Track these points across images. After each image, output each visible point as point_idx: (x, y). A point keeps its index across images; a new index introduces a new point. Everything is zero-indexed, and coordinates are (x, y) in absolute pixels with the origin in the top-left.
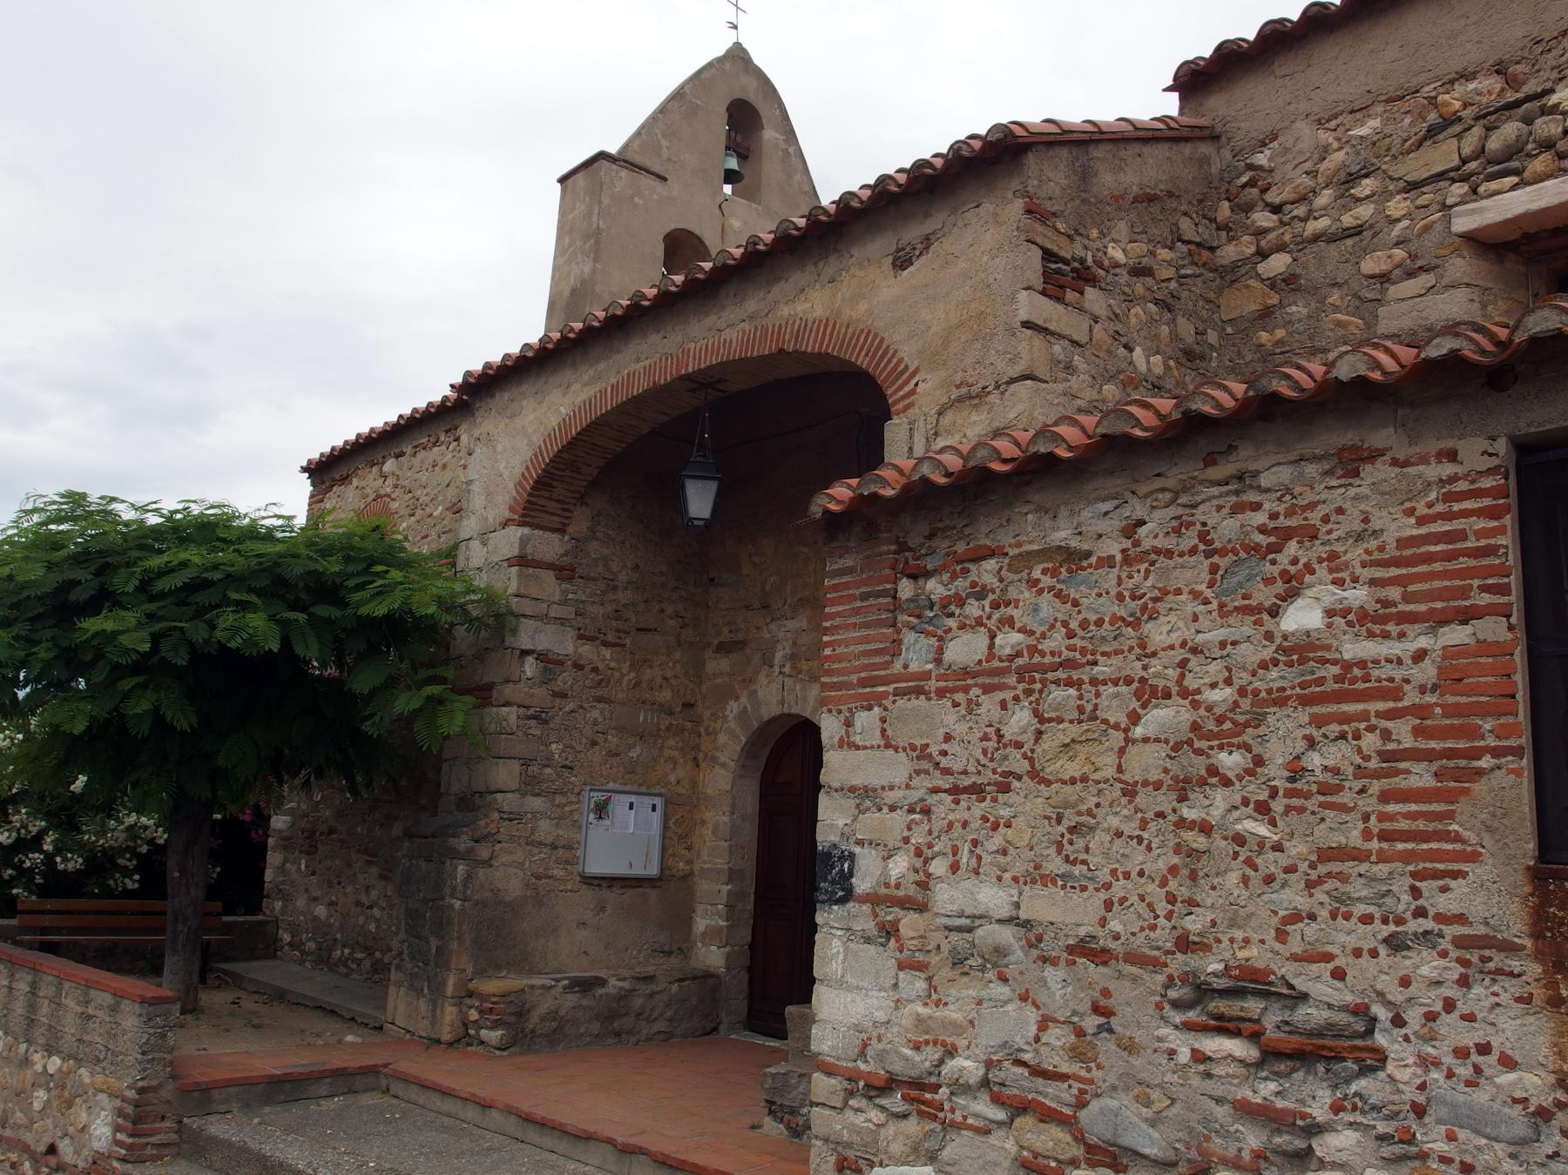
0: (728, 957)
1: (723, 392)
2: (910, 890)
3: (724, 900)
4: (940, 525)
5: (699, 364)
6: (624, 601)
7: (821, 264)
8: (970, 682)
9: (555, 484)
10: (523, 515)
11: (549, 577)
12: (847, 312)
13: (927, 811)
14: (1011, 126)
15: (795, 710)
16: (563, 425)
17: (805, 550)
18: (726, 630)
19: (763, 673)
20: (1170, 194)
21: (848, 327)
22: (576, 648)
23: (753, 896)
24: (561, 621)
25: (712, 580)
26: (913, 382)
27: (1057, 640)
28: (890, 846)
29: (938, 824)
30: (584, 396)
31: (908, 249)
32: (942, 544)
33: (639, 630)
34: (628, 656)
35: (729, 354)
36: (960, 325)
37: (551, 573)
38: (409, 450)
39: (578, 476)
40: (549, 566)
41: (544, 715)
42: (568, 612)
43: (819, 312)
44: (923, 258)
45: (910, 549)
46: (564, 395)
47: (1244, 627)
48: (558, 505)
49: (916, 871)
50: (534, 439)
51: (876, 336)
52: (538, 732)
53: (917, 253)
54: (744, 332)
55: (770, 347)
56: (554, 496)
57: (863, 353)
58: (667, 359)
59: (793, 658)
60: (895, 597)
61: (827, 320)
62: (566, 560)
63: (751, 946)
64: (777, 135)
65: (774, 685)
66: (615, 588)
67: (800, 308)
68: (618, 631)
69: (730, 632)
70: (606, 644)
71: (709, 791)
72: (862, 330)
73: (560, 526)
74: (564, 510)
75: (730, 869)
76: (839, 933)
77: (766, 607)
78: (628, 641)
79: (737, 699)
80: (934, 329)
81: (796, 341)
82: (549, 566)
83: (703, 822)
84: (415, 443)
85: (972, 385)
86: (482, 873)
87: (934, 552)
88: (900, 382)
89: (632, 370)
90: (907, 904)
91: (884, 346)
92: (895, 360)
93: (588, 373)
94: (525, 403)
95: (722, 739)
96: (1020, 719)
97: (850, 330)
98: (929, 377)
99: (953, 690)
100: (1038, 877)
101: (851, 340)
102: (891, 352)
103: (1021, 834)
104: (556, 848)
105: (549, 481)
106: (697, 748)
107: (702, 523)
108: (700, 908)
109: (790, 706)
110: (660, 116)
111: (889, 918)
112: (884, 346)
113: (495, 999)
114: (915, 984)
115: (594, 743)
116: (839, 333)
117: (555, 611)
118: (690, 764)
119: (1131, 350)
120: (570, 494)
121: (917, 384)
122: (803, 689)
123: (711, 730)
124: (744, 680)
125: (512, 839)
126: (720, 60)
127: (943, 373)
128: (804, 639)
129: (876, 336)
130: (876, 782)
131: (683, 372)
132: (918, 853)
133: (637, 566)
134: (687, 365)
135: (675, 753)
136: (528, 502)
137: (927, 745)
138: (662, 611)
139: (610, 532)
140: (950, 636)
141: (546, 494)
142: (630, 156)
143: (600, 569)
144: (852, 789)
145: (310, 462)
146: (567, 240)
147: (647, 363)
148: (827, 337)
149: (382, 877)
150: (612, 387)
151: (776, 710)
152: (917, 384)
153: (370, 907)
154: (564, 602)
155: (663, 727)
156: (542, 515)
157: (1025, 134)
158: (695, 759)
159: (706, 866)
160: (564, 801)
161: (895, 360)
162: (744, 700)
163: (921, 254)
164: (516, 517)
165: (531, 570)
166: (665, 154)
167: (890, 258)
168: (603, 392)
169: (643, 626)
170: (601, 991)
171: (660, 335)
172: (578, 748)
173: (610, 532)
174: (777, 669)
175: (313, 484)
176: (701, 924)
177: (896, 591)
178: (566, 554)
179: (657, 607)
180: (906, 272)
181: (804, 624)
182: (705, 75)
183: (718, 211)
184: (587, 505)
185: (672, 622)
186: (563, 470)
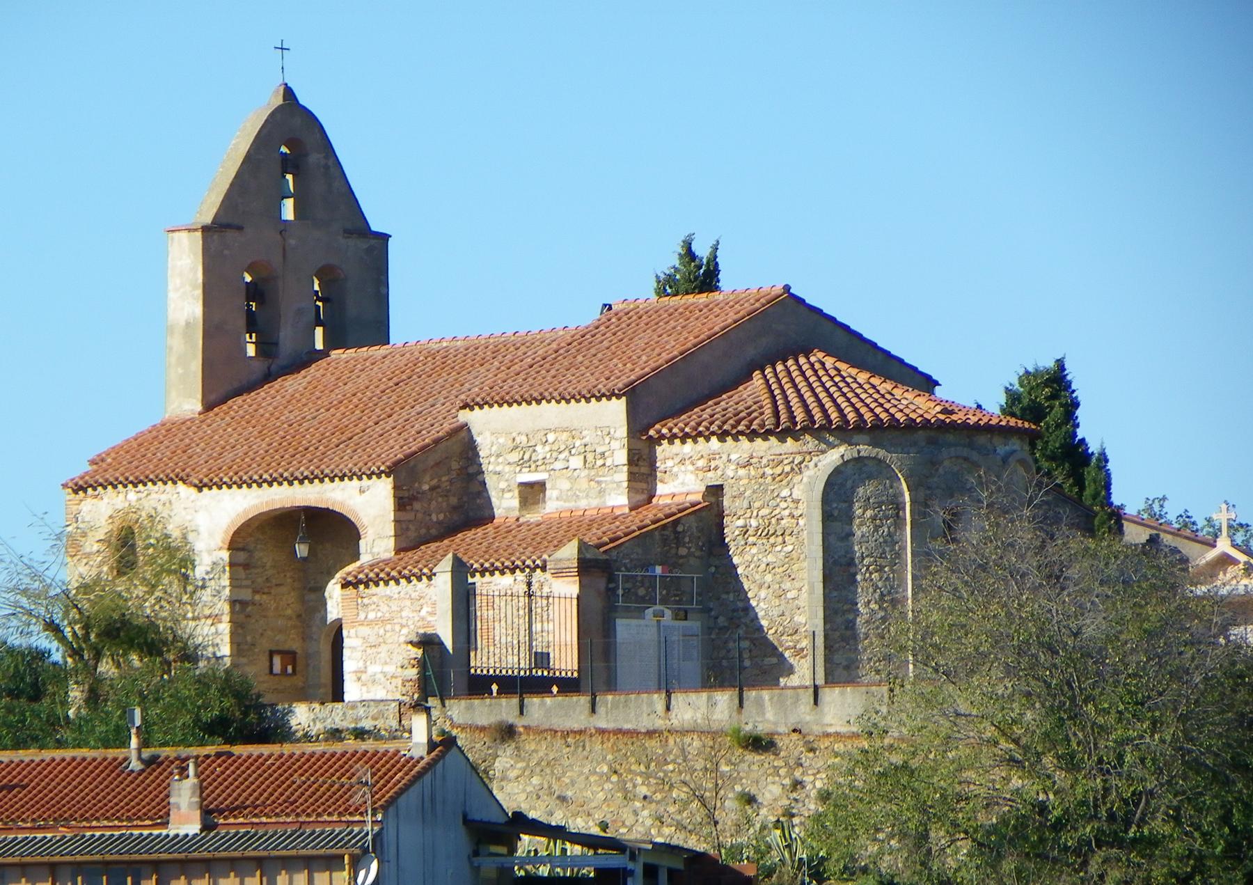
2: (363, 669)
11: (240, 569)
14: (836, 442)
20: (447, 458)
27: (387, 615)
47: (415, 614)
96: (382, 632)
100: (386, 663)
103: (383, 655)
114: (364, 689)
119: (430, 515)
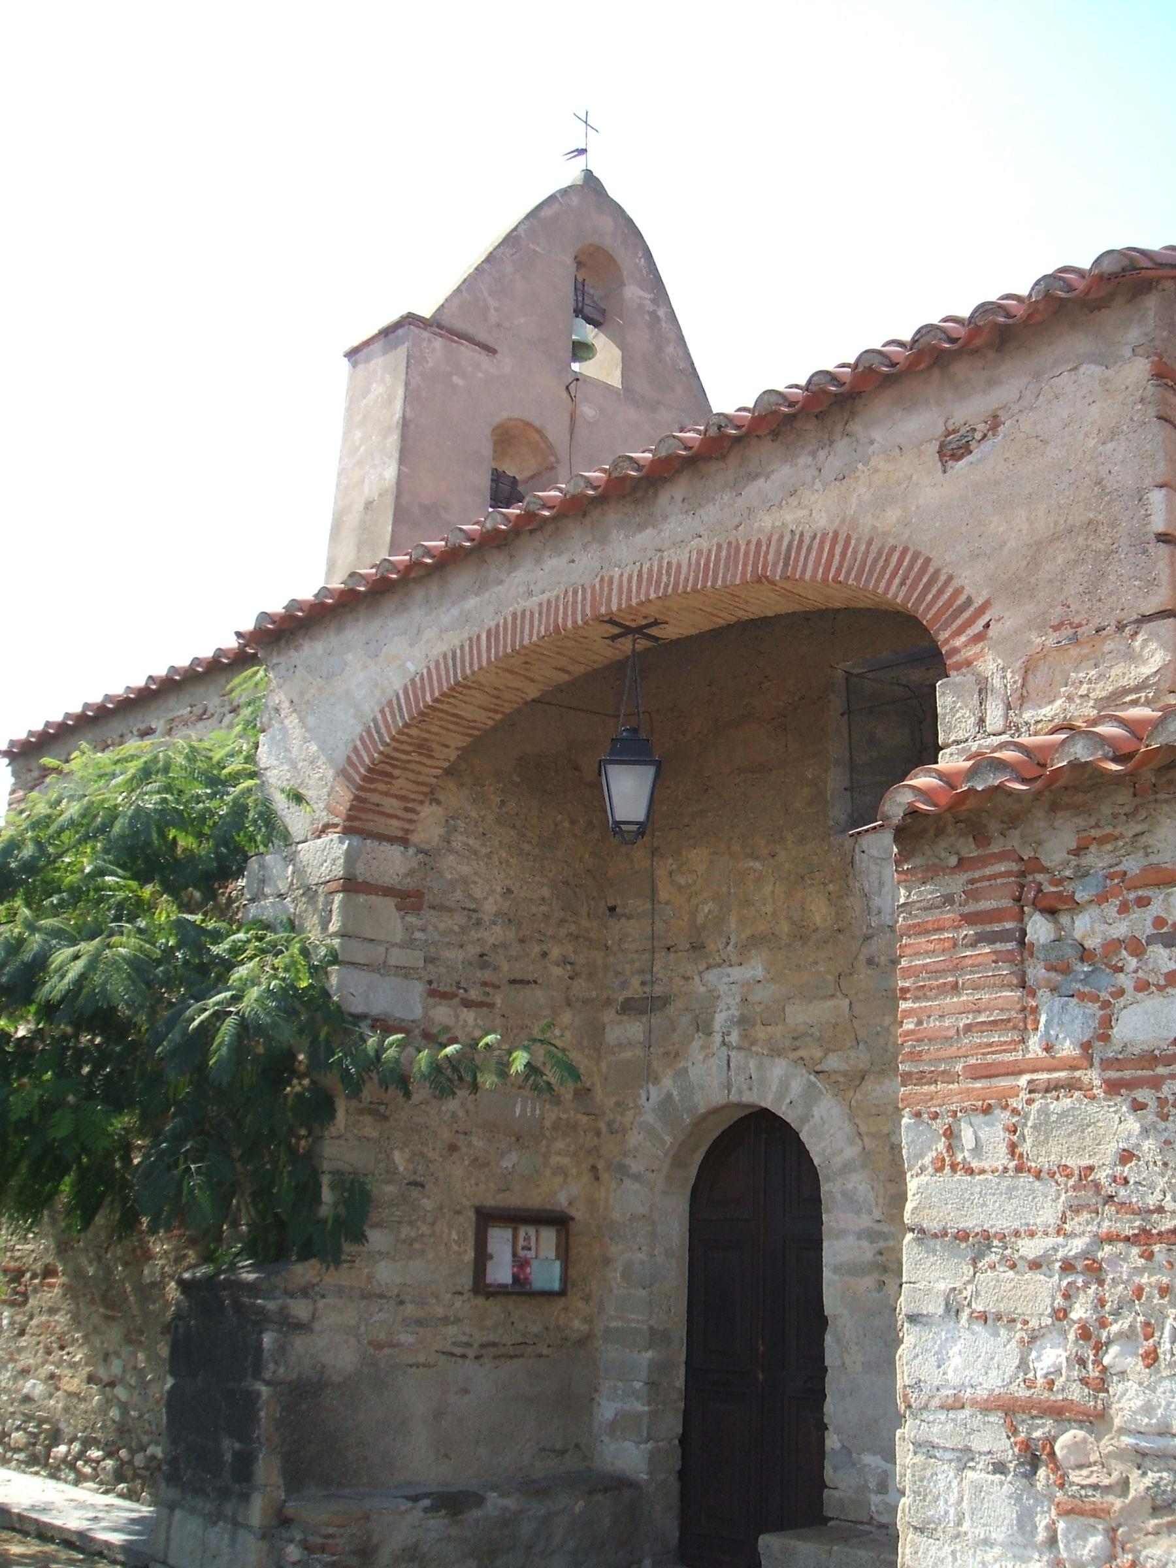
0: (652, 1457)
1: (656, 639)
3: (644, 1375)
4: (1094, 833)
5: (629, 598)
6: (492, 941)
7: (822, 454)
8: (1161, 1070)
9: (396, 772)
10: (350, 818)
11: (387, 905)
12: (867, 522)
13: (1095, 1271)
15: (750, 1097)
16: (414, 686)
17: (758, 865)
18: (635, 981)
19: (696, 1044)
21: (869, 544)
22: (426, 1009)
23: (682, 1370)
24: (405, 972)
25: (612, 909)
26: (982, 622)
28: (1033, 1323)
29: (1113, 1294)
30: (441, 648)
31: (963, 431)
32: (1097, 860)
33: (513, 982)
34: (498, 1021)
35: (676, 584)
36: (1054, 538)
37: (390, 902)
38: (159, 724)
39: (428, 762)
40: (388, 891)
41: (382, 1108)
42: (415, 958)
43: (822, 521)
44: (986, 446)
45: (1045, 870)
46: (412, 645)
48: (401, 804)
49: (1082, 1362)
50: (366, 708)
51: (916, 556)
52: (375, 1134)
53: (978, 436)
54: (700, 552)
55: (744, 574)
56: (394, 790)
57: (897, 581)
58: (575, 593)
59: (744, 1022)
60: (1022, 943)
61: (836, 534)
62: (410, 884)
63: (684, 1440)
64: (641, 293)
65: (713, 1061)
66: (479, 923)
67: (790, 517)
68: (484, 984)
69: (643, 983)
70: (467, 1004)
71: (616, 1215)
72: (894, 548)
73: (400, 834)
74: (406, 809)
75: (651, 1328)
76: (949, 1455)
77: (697, 947)
78: (498, 1000)
79: (656, 1080)
80: (1012, 544)
81: (786, 564)
82: (388, 891)
83: (607, 1261)
84: (170, 716)
85: (1080, 625)
86: (299, 1342)
87: (1086, 874)
88: (959, 622)
89: (519, 610)
90: (1060, 1413)
91: (931, 570)
92: (949, 591)
93: (448, 615)
94: (349, 657)
95: (634, 1139)
97: (874, 548)
98: (1007, 614)
99: (1131, 1085)
101: (876, 561)
102: (943, 578)
104: (402, 1303)
105: (388, 769)
106: (595, 1151)
107: (634, 828)
108: (606, 1386)
109: (740, 1091)
110: (485, 266)
111: (1037, 1434)
112: (931, 570)
113: (330, 1530)
115: (453, 1148)
116: (855, 552)
117: (398, 957)
118: (586, 1178)
120: (415, 787)
121: (987, 626)
122: (760, 1066)
123: (616, 1126)
124: (667, 1054)
125: (340, 1291)
126: (565, 192)
127: (1031, 608)
128: (761, 994)
129: (916, 556)
130: (1000, 1224)
131: (603, 610)
132: (1085, 1334)
133: (509, 891)
134: (609, 601)
135: (566, 1161)
136: (357, 798)
137: (1091, 1168)
138: (545, 954)
139: (471, 842)
140: (1122, 1001)
141: (382, 787)
142: (446, 321)
143: (458, 895)
144: (963, 1236)
145: (12, 743)
146: (359, 435)
147: (544, 598)
148: (837, 558)
149: (128, 1340)
150: (489, 632)
151: (718, 1098)
152: (987, 626)
153: (112, 1384)
154: (409, 944)
155: (548, 1123)
156: (376, 818)
157: (1150, 265)
158: (594, 1168)
159: (614, 1324)
160: (413, 1234)
161: (949, 591)
162: (667, 1082)
163: (985, 436)
164: (336, 820)
165: (362, 898)
166: (493, 317)
167: (935, 446)
168: (474, 641)
169: (518, 975)
170: (476, 1513)
171: (565, 558)
172: (432, 1155)
173: (471, 842)
174: (717, 1038)
175: (15, 774)
176: (607, 1410)
177: (1024, 933)
178: (411, 873)
179: (537, 949)
180: (962, 463)
181: (759, 972)
182: (546, 213)
183: (565, 394)
184: (439, 803)
185: (557, 971)
186: (408, 753)
